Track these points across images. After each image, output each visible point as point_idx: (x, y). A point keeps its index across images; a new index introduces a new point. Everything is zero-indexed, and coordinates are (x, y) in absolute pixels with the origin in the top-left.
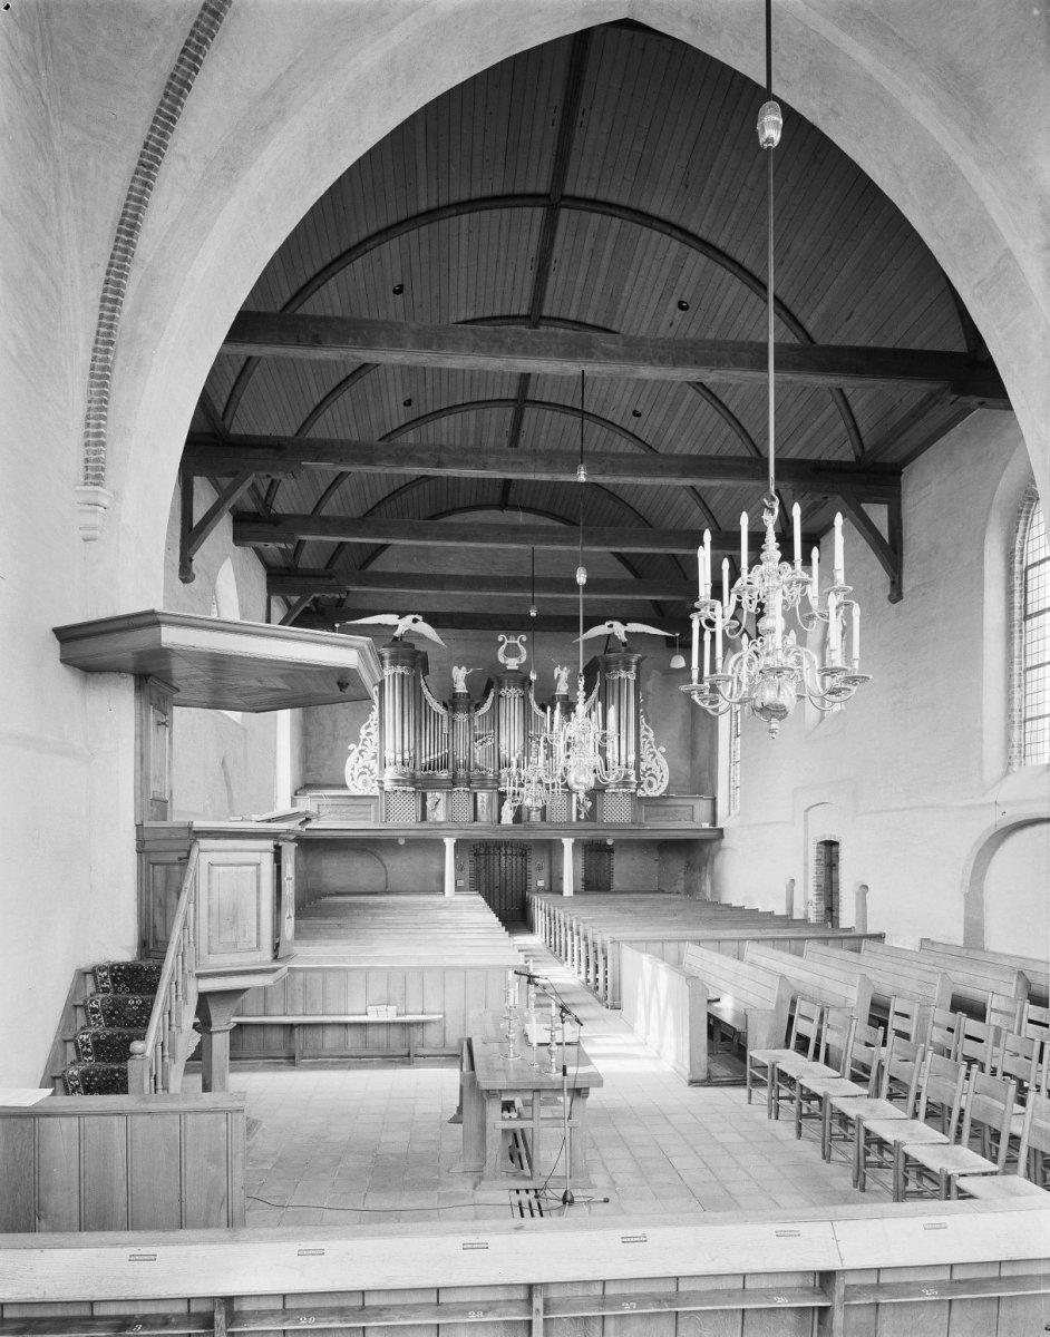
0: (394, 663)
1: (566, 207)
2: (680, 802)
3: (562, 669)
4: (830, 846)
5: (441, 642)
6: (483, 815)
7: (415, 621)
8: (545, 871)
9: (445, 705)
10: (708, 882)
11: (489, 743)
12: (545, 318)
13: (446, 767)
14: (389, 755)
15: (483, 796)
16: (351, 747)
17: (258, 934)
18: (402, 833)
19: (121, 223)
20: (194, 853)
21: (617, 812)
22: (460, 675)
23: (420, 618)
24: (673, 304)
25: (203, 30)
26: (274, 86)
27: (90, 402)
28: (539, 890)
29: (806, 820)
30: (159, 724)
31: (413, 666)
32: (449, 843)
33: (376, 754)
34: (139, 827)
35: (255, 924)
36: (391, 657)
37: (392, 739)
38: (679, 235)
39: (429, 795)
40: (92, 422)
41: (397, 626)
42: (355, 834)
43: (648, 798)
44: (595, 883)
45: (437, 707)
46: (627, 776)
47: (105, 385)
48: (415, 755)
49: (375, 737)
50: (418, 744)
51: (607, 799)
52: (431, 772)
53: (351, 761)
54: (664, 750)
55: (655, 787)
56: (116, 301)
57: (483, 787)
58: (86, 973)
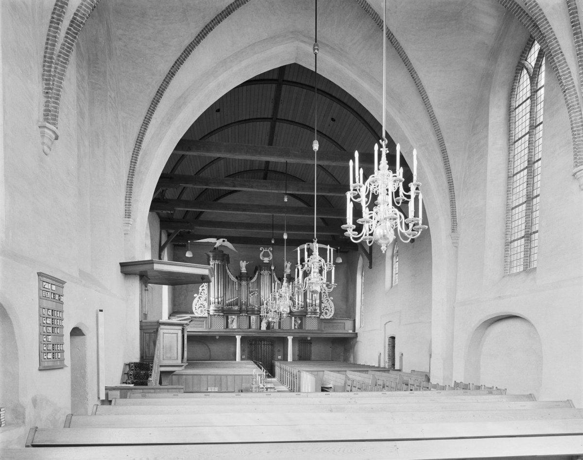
0: (214, 259)
1: (285, 84)
2: (339, 321)
3: (288, 263)
4: (393, 338)
5: (234, 249)
6: (254, 327)
7: (224, 241)
8: (281, 353)
9: (237, 278)
10: (352, 356)
11: (256, 295)
12: (279, 119)
13: (237, 305)
14: (212, 299)
15: (253, 318)
16: (195, 295)
17: (177, 355)
18: (217, 333)
19: (138, 139)
20: (159, 329)
21: (311, 325)
22: (243, 264)
23: (226, 240)
24: (329, 118)
25: (164, 86)
26: (183, 95)
27: (127, 192)
28: (278, 360)
29: (385, 328)
30: (145, 290)
31: (223, 260)
32: (238, 338)
33: (205, 302)
34: (141, 322)
35: (176, 352)
36: (213, 257)
37: (213, 292)
38: (329, 96)
39: (230, 317)
40: (128, 198)
41: (216, 243)
42: (197, 333)
43: (325, 319)
44: (303, 357)
45: (233, 278)
46: (316, 310)
47: (131, 187)
49: (206, 291)
50: (225, 294)
51: (307, 320)
52: (230, 307)
54: (332, 298)
55: (328, 314)
56: (135, 165)
57: (253, 314)
58: (127, 365)
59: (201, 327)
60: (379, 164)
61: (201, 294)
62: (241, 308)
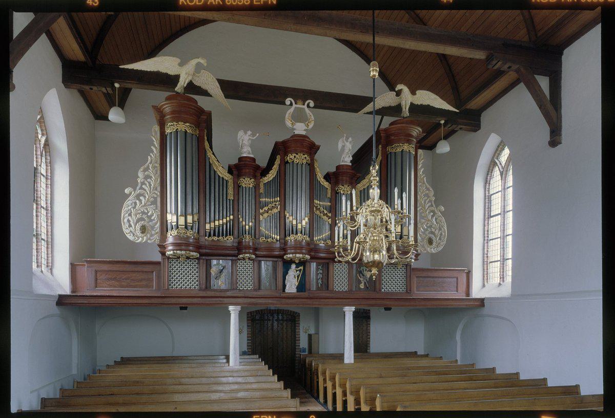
9: (230, 171)
16: (127, 191)
39: (214, 262)
48: (198, 219)
52: (216, 238)
53: (127, 205)
59: (147, 286)
60: (133, 291)
61: (141, 188)
62: (240, 243)
